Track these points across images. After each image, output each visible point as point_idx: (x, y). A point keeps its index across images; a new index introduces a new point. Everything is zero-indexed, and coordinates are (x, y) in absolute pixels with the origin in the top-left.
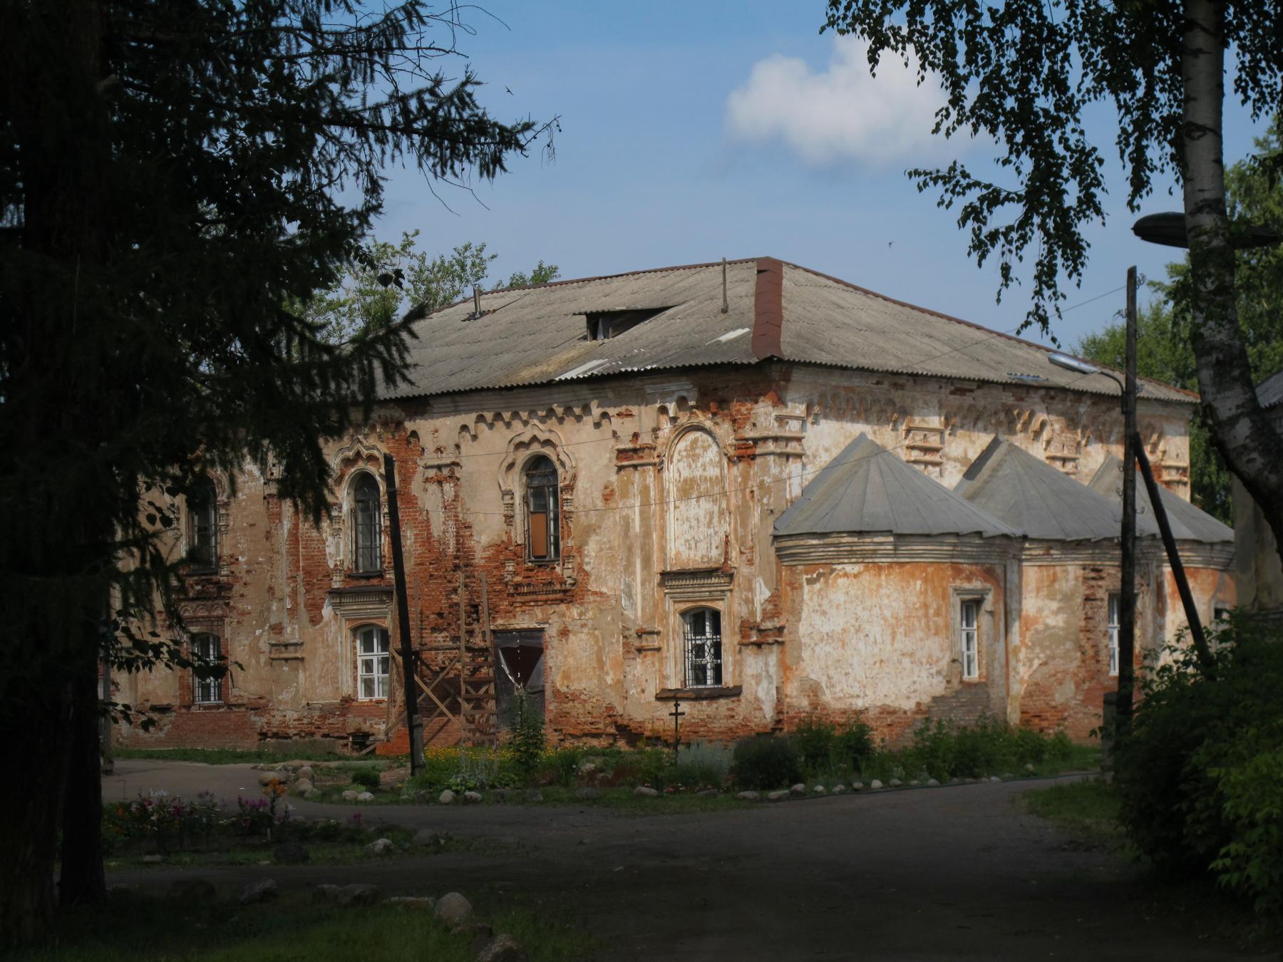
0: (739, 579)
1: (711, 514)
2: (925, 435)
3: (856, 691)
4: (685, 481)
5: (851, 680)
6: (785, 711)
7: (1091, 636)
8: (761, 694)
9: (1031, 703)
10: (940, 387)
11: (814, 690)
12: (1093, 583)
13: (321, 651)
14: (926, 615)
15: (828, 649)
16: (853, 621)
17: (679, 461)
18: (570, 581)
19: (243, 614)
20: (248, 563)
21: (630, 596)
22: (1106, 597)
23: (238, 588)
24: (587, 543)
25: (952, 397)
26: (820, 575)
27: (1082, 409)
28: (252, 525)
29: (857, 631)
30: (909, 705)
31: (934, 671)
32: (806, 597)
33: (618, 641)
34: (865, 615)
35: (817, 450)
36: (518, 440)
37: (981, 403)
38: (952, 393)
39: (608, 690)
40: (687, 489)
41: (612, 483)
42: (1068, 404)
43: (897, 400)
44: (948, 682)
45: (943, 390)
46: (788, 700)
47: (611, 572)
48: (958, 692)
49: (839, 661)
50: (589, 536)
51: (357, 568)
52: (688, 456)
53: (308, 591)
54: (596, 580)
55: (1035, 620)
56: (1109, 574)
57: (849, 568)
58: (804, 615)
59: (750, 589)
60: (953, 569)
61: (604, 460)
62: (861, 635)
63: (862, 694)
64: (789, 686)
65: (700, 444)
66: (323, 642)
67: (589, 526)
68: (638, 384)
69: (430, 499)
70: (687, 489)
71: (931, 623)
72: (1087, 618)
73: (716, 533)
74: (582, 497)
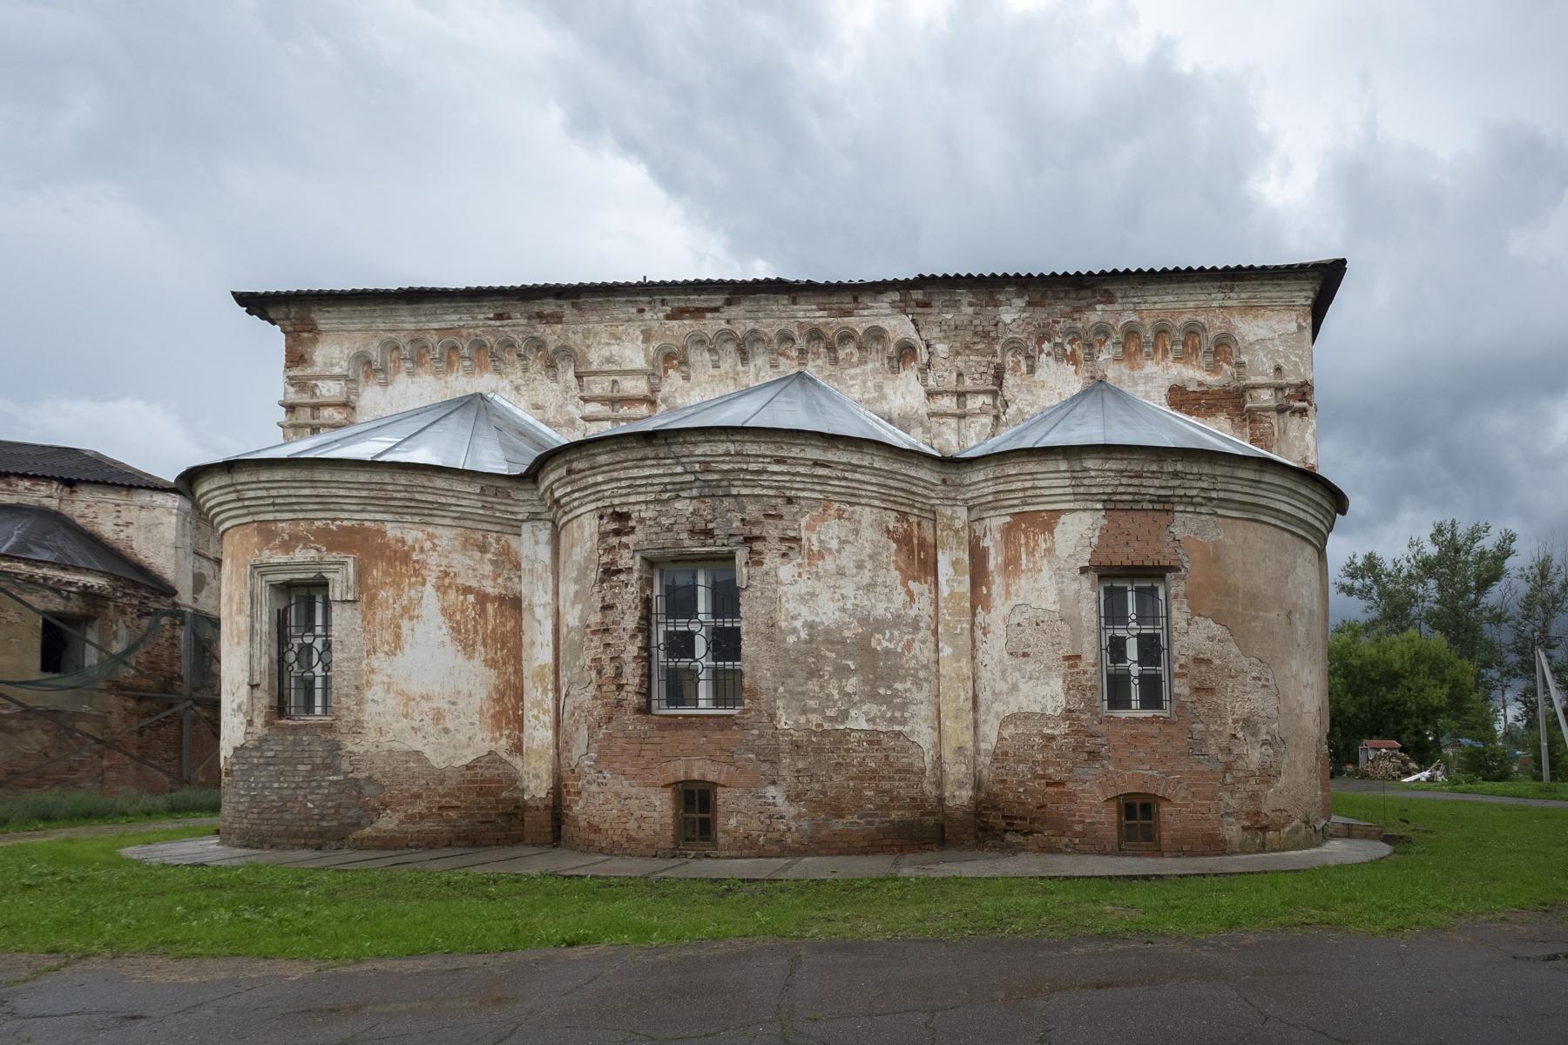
7: (609, 640)
10: (641, 311)
12: (614, 541)
22: (637, 563)
25: (674, 323)
27: (1008, 315)
38: (668, 317)
44: (250, 723)
48: (263, 740)
56: (641, 521)
60: (260, 532)
72: (606, 608)
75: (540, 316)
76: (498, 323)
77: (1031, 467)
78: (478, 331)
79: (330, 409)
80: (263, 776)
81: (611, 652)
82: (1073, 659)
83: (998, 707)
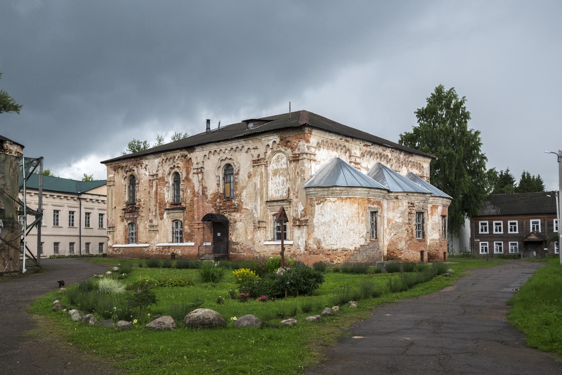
7: (410, 226)
10: (360, 143)
12: (411, 208)
38: (364, 146)
56: (416, 205)
75: (346, 140)
76: (340, 140)
77: (438, 199)
78: (336, 141)
79: (313, 155)
80: (369, 251)
81: (411, 228)
82: (440, 230)
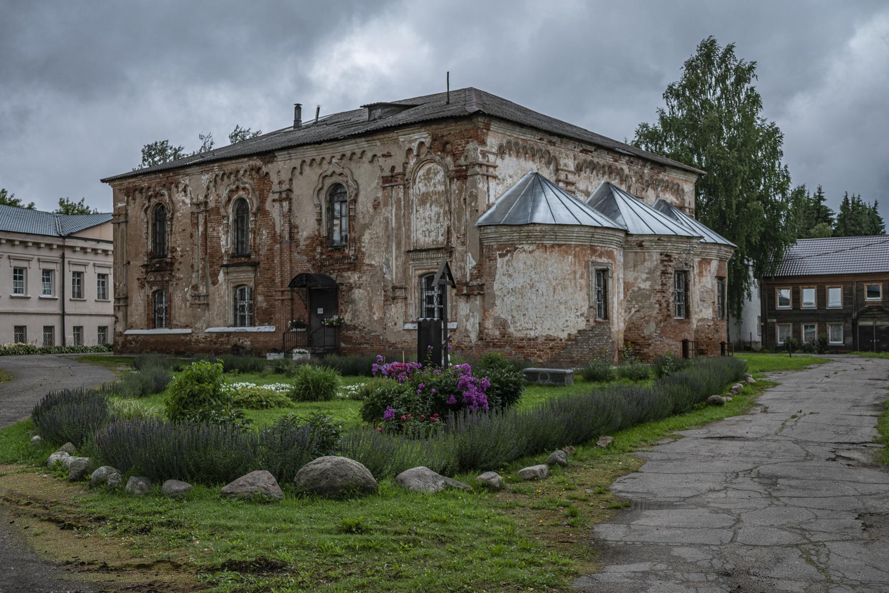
0: (457, 254)
1: (439, 214)
2: (566, 175)
3: (530, 326)
4: (423, 194)
5: (527, 318)
6: (484, 338)
7: (664, 295)
8: (469, 327)
9: (630, 335)
11: (503, 325)
12: (666, 263)
13: (218, 300)
14: (575, 278)
15: (512, 298)
16: (528, 281)
17: (419, 182)
18: (353, 258)
19: (179, 279)
20: (181, 251)
21: (388, 267)
23: (176, 265)
24: (363, 235)
25: (580, 154)
26: (508, 252)
28: (184, 230)
29: (531, 287)
30: (564, 336)
31: (579, 314)
32: (499, 265)
33: (381, 295)
34: (536, 278)
35: (505, 176)
36: (324, 174)
37: (596, 160)
38: (581, 152)
39: (375, 323)
40: (424, 199)
41: (379, 198)
42: (639, 167)
43: (551, 152)
44: (588, 321)
45: (576, 149)
46: (486, 331)
47: (378, 252)
49: (519, 306)
50: (365, 230)
51: (238, 252)
52: (425, 179)
53: (211, 267)
54: (368, 257)
55: (633, 285)
56: (675, 258)
57: (526, 247)
58: (497, 277)
59: (463, 260)
61: (374, 185)
62: (534, 290)
63: (534, 328)
64: (487, 322)
65: (432, 171)
66: (219, 294)
67: (365, 224)
68: (393, 135)
69: (275, 211)
70: (424, 199)
71: (578, 283)
73: (442, 226)
74: (361, 207)
78: (532, 143)
83: (696, 316)
